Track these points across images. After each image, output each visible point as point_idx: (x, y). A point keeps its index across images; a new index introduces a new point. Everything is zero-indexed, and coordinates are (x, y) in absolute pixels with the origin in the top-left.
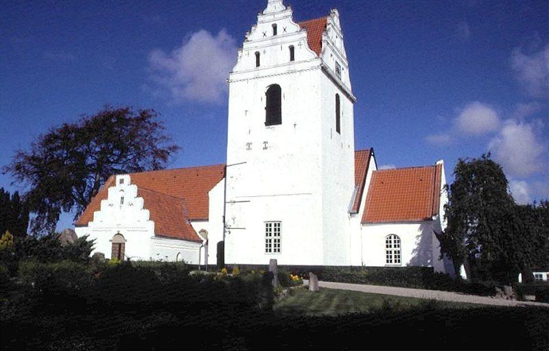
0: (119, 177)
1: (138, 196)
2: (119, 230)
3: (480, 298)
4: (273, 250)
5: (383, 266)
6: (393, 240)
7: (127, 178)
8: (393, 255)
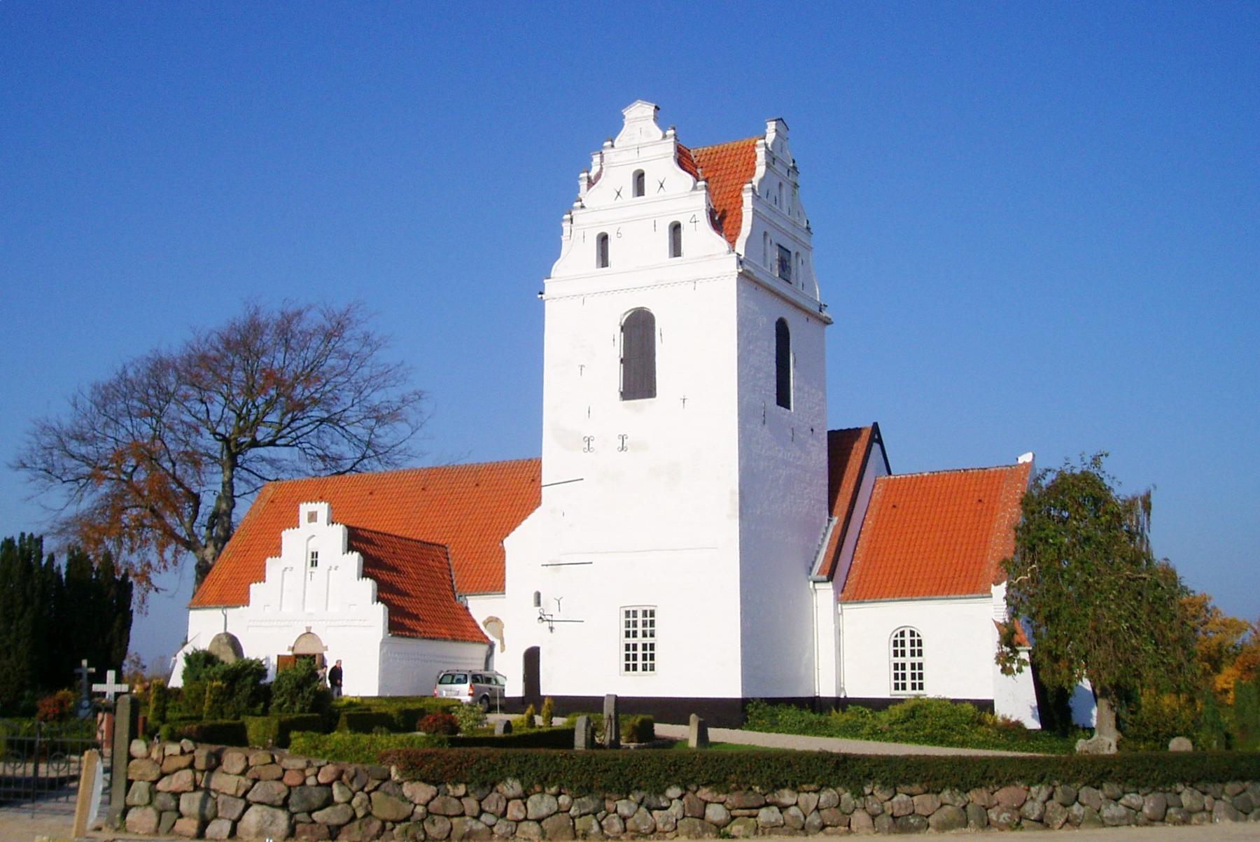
0: (305, 509)
1: (350, 548)
2: (308, 625)
3: (789, 746)
4: (640, 667)
5: (887, 696)
6: (907, 638)
7: (322, 509)
8: (908, 671)
